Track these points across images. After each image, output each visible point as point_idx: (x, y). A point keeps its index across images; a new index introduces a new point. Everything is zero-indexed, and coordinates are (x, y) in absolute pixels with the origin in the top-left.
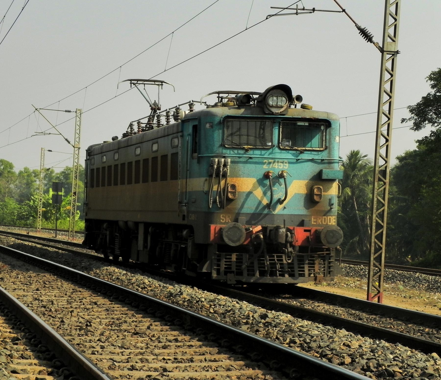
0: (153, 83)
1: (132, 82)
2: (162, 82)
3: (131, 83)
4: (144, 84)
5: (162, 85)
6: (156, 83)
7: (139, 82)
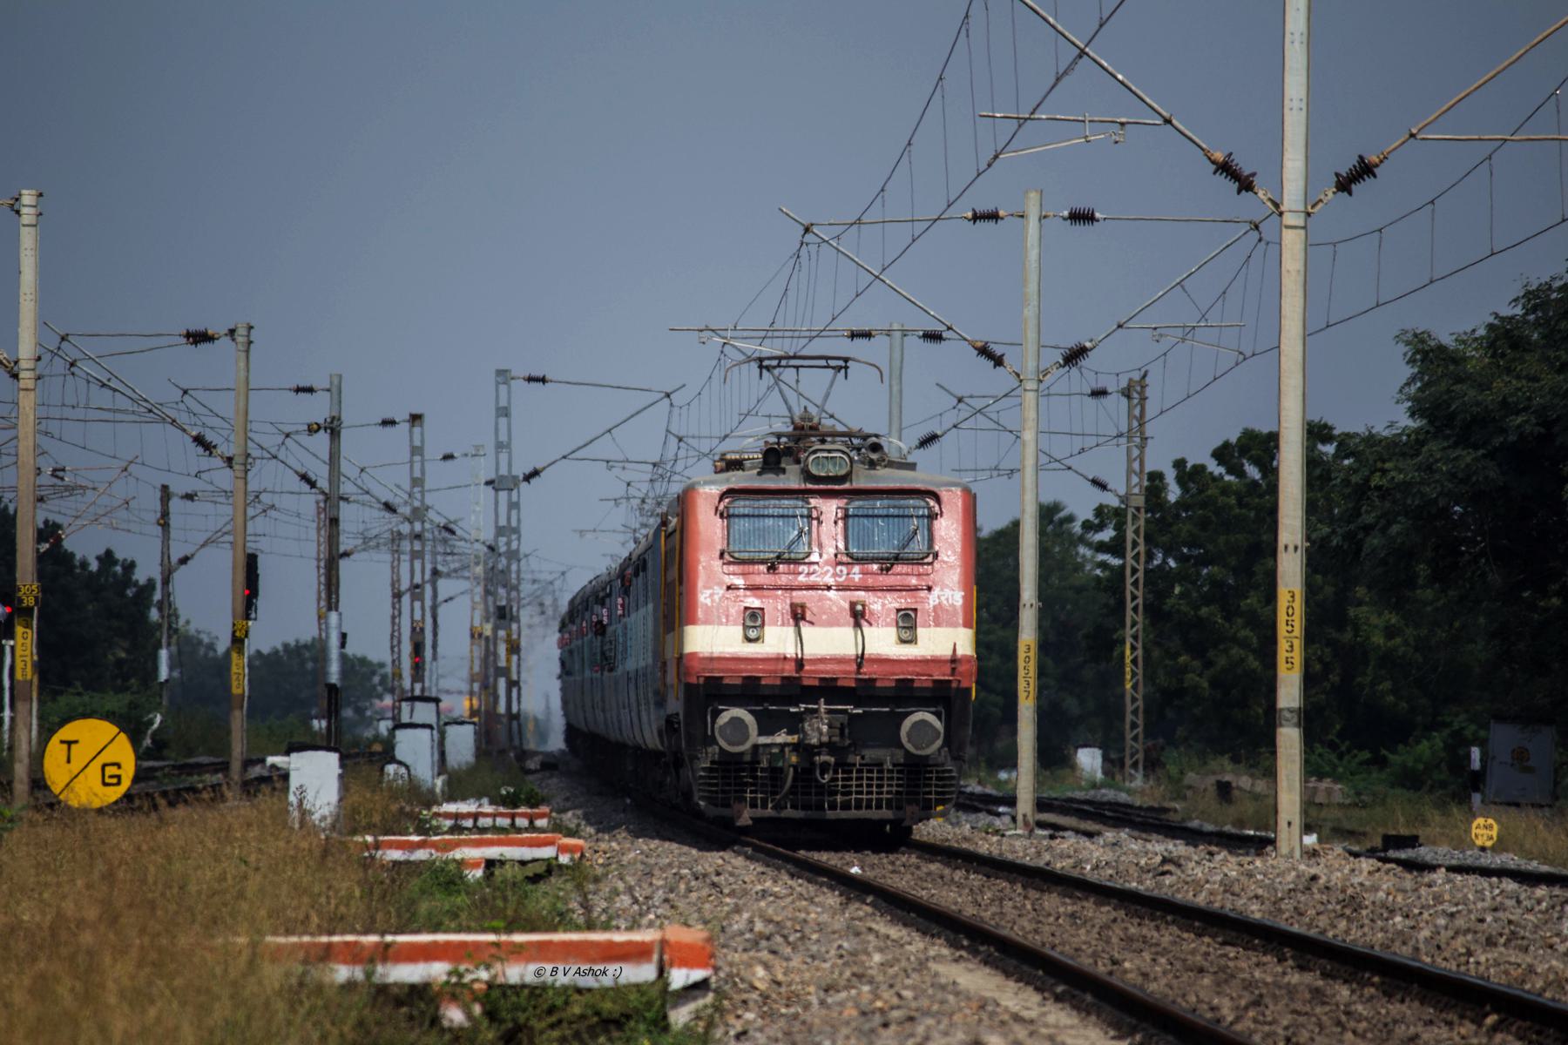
0: (823, 363)
1: (766, 363)
2: (846, 360)
3: (761, 367)
4: (797, 367)
5: (846, 368)
6: (832, 363)
7: (784, 363)
